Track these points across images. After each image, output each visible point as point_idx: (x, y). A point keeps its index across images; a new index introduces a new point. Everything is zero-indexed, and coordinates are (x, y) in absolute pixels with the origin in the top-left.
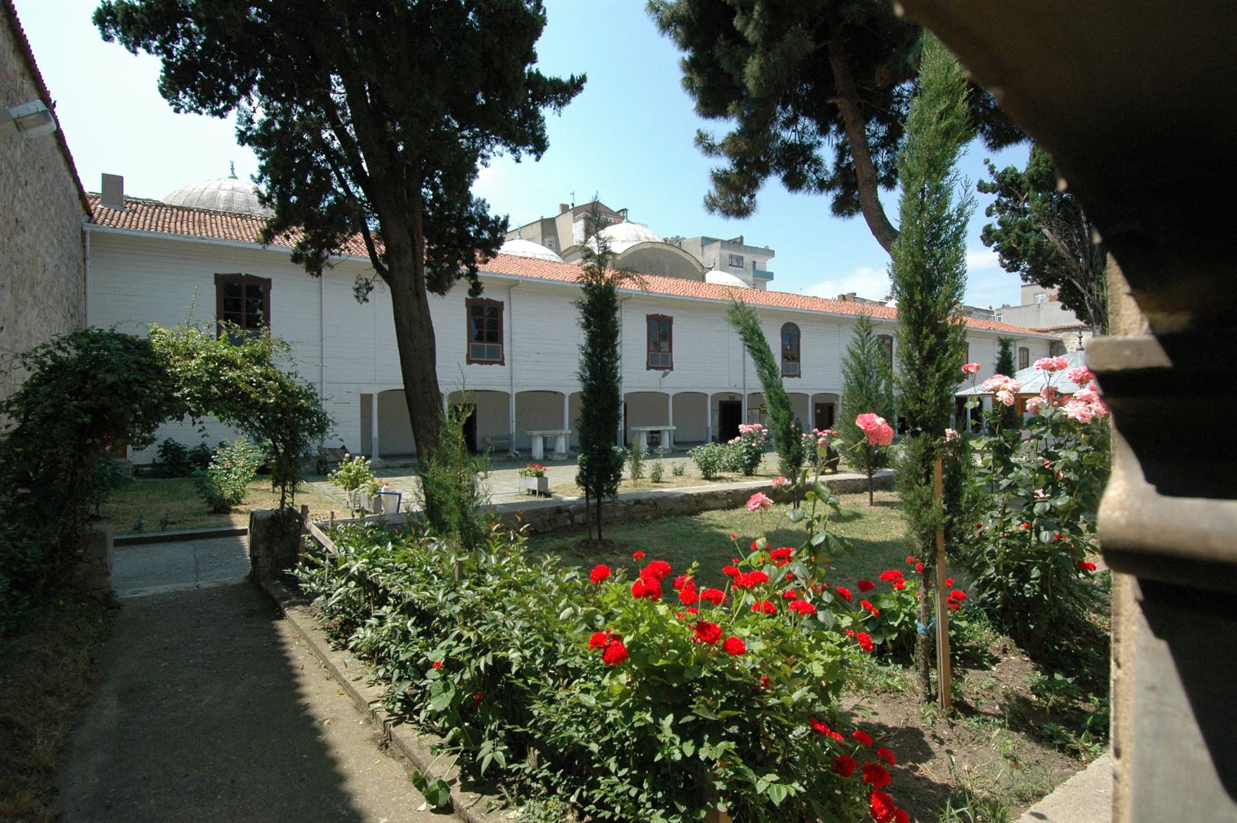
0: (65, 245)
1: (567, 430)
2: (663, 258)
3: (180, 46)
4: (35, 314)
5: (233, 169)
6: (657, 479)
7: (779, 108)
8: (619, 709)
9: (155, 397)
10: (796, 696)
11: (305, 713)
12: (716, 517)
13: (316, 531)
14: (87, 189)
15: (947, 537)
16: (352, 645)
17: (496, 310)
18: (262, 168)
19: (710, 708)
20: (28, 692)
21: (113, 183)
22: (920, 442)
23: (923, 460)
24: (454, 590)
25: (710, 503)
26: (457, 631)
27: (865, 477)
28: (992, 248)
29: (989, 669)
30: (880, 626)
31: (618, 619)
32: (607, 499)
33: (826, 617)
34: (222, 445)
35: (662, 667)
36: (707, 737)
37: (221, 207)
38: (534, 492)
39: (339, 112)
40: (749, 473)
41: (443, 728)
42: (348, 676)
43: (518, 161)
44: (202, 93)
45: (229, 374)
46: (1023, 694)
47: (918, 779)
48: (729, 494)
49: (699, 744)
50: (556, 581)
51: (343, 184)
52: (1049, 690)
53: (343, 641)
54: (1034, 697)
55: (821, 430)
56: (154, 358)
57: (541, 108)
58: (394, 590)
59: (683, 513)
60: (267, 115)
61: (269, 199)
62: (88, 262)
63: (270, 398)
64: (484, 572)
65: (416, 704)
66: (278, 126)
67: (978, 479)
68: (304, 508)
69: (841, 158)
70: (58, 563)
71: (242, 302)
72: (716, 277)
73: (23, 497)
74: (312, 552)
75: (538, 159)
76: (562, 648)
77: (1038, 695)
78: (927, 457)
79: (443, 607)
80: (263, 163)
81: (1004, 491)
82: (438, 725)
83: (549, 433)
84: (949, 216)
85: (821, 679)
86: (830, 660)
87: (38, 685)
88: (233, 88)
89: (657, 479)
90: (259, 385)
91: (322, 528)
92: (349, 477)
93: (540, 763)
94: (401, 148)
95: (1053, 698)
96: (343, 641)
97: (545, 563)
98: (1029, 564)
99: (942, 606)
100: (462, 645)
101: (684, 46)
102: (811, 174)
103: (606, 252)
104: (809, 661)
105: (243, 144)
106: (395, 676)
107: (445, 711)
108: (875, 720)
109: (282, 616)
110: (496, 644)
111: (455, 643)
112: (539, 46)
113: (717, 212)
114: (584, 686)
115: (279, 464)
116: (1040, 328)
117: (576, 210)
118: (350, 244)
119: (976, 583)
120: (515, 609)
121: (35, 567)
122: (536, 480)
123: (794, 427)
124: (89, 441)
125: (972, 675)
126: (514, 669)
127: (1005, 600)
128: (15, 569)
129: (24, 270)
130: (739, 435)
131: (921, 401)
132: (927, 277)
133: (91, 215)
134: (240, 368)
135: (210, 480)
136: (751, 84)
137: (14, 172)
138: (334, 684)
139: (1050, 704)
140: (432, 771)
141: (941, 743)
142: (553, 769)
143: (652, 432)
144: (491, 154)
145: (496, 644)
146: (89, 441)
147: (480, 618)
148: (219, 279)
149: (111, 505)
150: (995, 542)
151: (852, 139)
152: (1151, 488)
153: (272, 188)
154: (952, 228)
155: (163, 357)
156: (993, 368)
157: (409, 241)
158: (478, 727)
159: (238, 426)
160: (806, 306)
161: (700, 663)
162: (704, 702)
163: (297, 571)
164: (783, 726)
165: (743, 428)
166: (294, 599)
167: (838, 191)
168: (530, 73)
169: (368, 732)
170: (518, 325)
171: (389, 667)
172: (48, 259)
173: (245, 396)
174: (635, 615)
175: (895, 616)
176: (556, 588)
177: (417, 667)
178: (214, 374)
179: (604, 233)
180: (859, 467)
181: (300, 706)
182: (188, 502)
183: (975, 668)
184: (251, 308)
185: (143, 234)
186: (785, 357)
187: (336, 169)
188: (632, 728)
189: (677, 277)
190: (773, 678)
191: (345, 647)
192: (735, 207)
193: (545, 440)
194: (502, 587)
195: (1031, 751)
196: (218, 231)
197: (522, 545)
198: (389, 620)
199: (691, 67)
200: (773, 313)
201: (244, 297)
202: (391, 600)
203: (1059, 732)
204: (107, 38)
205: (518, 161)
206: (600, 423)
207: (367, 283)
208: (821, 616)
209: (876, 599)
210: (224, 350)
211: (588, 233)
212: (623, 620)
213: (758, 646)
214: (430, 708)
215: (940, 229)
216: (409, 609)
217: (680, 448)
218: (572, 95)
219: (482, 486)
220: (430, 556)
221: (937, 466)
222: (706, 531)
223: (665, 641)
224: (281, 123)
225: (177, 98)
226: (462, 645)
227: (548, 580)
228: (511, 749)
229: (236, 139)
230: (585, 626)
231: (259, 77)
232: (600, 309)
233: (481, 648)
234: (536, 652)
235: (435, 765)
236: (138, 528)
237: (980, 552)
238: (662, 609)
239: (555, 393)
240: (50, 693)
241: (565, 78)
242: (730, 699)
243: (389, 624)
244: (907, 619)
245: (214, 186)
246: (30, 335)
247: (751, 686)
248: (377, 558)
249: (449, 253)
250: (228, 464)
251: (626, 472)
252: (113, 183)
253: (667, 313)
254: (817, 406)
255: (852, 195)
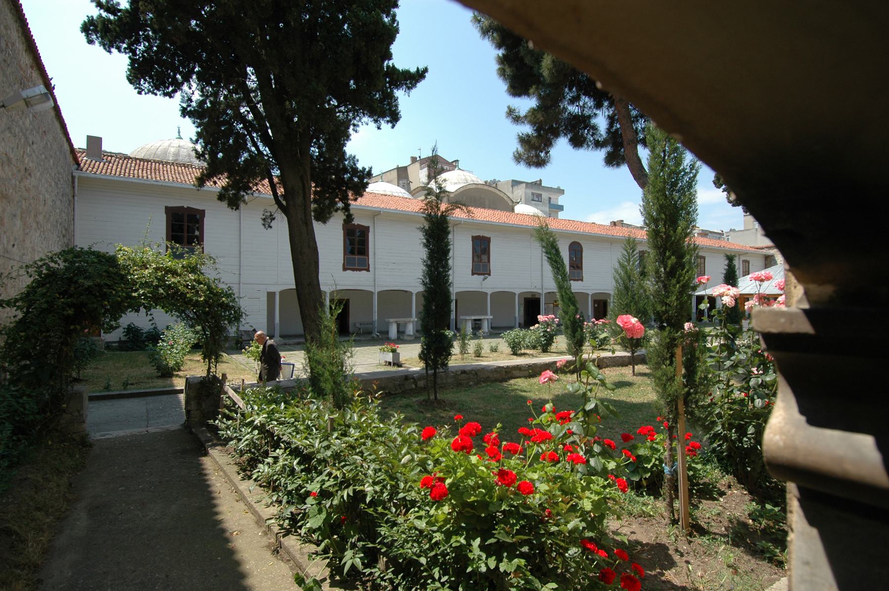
0: (60, 186)
1: (414, 318)
2: (484, 195)
3: (142, 47)
4: (37, 235)
5: (179, 132)
6: (478, 354)
7: (567, 90)
8: (442, 532)
9: (119, 296)
10: (570, 526)
11: (220, 526)
12: (520, 383)
13: (231, 393)
14: (76, 146)
15: (686, 403)
16: (254, 477)
17: (364, 232)
18: (198, 133)
19: (508, 534)
20: (24, 509)
21: (94, 142)
22: (666, 334)
23: (668, 348)
24: (327, 439)
25: (516, 373)
26: (328, 470)
27: (629, 354)
28: (721, 189)
29: (718, 500)
30: (638, 467)
31: (443, 464)
32: (441, 370)
33: (596, 463)
34: (167, 328)
35: (474, 501)
36: (505, 554)
37: (171, 159)
38: (390, 363)
39: (252, 95)
40: (545, 350)
41: (318, 540)
42: (251, 500)
43: (379, 128)
44: (157, 80)
45: (172, 280)
46: (742, 519)
47: (664, 582)
48: (530, 366)
49: (499, 560)
50: (400, 434)
51: (255, 145)
52: (762, 516)
53: (249, 473)
54: (751, 521)
55: (597, 320)
56: (119, 269)
57: (395, 91)
58: (285, 438)
59: (496, 380)
60: (201, 96)
61: (203, 155)
62: (76, 198)
63: (201, 297)
64: (349, 426)
65: (299, 521)
66: (209, 105)
67: (709, 360)
68: (224, 375)
69: (611, 125)
70: (48, 414)
71: (184, 227)
72: (523, 209)
73: (26, 367)
74: (228, 408)
75: (393, 127)
76: (402, 485)
77: (754, 520)
78: (671, 345)
79: (318, 452)
80: (199, 130)
81: (728, 369)
82: (315, 536)
83: (401, 320)
84: (684, 170)
85: (590, 512)
86: (596, 498)
87: (31, 504)
88: (179, 76)
89: (478, 354)
90: (193, 287)
91: (235, 390)
92: (258, 352)
93: (387, 568)
94: (296, 119)
95: (764, 523)
96: (249, 473)
97: (393, 419)
98: (747, 423)
99: (683, 454)
100: (332, 480)
101: (499, 46)
102: (589, 136)
103: (442, 191)
104: (580, 498)
105: (184, 117)
106: (284, 501)
107: (319, 528)
108: (633, 537)
109: (206, 454)
110: (355, 480)
111: (327, 478)
112: (394, 48)
113: (522, 163)
114: (417, 515)
115: (207, 343)
116: (757, 246)
117: (422, 161)
118: (260, 187)
119: (708, 436)
120: (370, 455)
121: (31, 417)
122: (391, 354)
123: (579, 318)
124: (72, 327)
125: (705, 504)
126: (368, 499)
127: (729, 449)
128: (17, 418)
129: (30, 204)
130: (538, 323)
131: (666, 304)
132: (670, 211)
133: (79, 165)
134: (180, 275)
135: (158, 353)
136: (546, 73)
137: (24, 135)
138: (241, 506)
139: (762, 526)
140: (309, 572)
141: (682, 555)
142: (396, 573)
143: (475, 320)
144: (360, 123)
145: (355, 480)
146: (72, 327)
147: (346, 461)
148: (168, 210)
149: (88, 371)
150: (721, 407)
151: (619, 112)
152: (803, 419)
153: (205, 147)
154: (686, 178)
155: (125, 267)
156: (722, 277)
157: (301, 185)
158: (344, 539)
159: (178, 317)
160: (587, 230)
161: (501, 499)
162: (503, 529)
163: (217, 422)
164: (561, 547)
165: (541, 318)
166: (215, 442)
167: (609, 149)
168: (388, 67)
169: (265, 541)
170: (380, 243)
171: (280, 494)
172: (47, 196)
173: (183, 295)
174: (454, 462)
175: (648, 460)
176: (399, 439)
177: (300, 495)
178: (161, 280)
179: (444, 176)
180: (625, 348)
181: (217, 521)
182: (143, 369)
183: (707, 499)
184: (191, 230)
185: (116, 178)
186: (571, 266)
187: (250, 134)
188: (451, 546)
189: (494, 209)
190: (554, 512)
191: (250, 478)
192: (535, 160)
193: (398, 325)
194: (362, 437)
195: (748, 563)
196: (168, 176)
197: (377, 407)
198: (281, 460)
199: (504, 60)
200: (565, 235)
201: (186, 224)
202: (282, 445)
203: (768, 548)
204: (91, 42)
205: (379, 128)
206: (437, 314)
207: (271, 215)
208: (592, 462)
209: (635, 447)
210: (169, 263)
211: (430, 177)
212: (446, 466)
213: (543, 487)
214: (308, 525)
215: (677, 180)
216: (295, 452)
217: (496, 331)
218: (417, 81)
219: (348, 362)
220: (311, 413)
221: (678, 351)
222: (513, 394)
223: (476, 483)
224: (211, 102)
225: (139, 84)
226: (332, 480)
227: (394, 432)
228: (366, 556)
229: (180, 113)
230: (419, 469)
231: (197, 69)
232: (437, 233)
233: (345, 483)
234: (384, 487)
235: (312, 567)
236: (107, 388)
237: (711, 413)
238: (474, 459)
239: (406, 292)
240: (38, 509)
241: (413, 70)
242: (522, 527)
243: (281, 462)
244: (657, 462)
245: (166, 144)
246: (33, 249)
247: (538, 516)
248: (273, 414)
249: (330, 193)
250: (171, 342)
251: (456, 349)
252: (94, 142)
253: (487, 235)
254: (595, 302)
255: (618, 151)
